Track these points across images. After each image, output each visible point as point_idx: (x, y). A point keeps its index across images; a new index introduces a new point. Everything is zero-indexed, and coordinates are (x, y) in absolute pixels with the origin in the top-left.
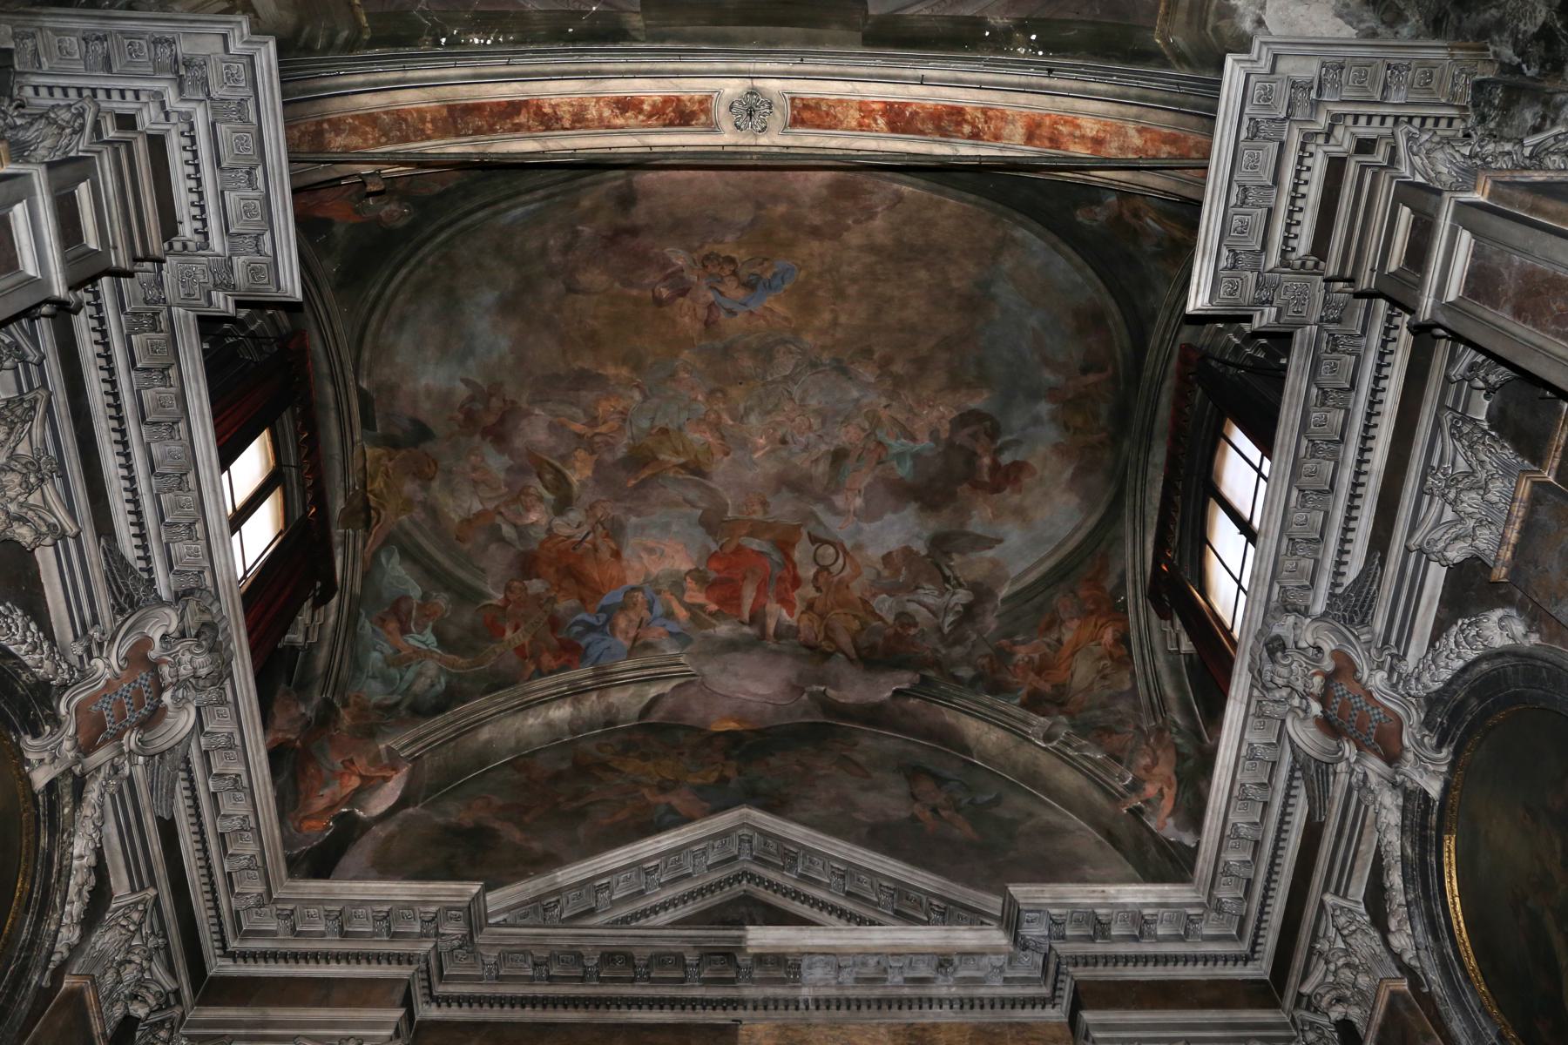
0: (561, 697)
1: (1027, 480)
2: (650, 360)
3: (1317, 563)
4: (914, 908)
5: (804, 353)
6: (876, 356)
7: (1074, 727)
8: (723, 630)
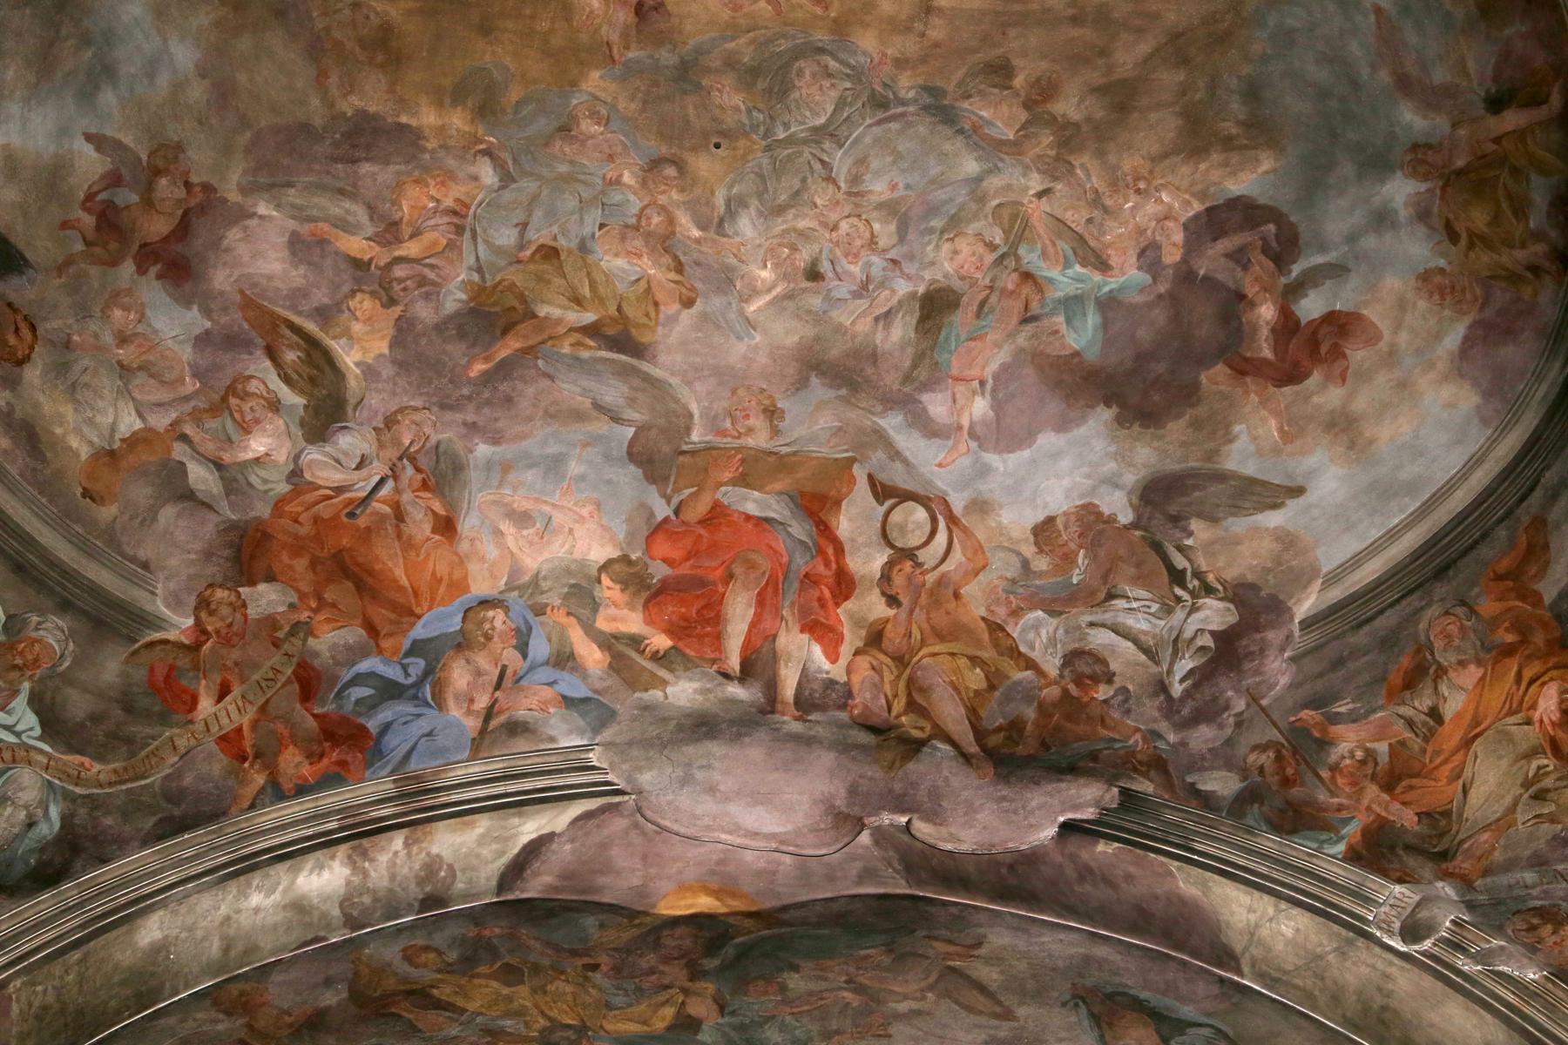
0: (327, 843)
1: (1357, 355)
2: (514, 94)
5: (857, 75)
6: (1019, 81)
7: (1470, 906)
8: (684, 692)
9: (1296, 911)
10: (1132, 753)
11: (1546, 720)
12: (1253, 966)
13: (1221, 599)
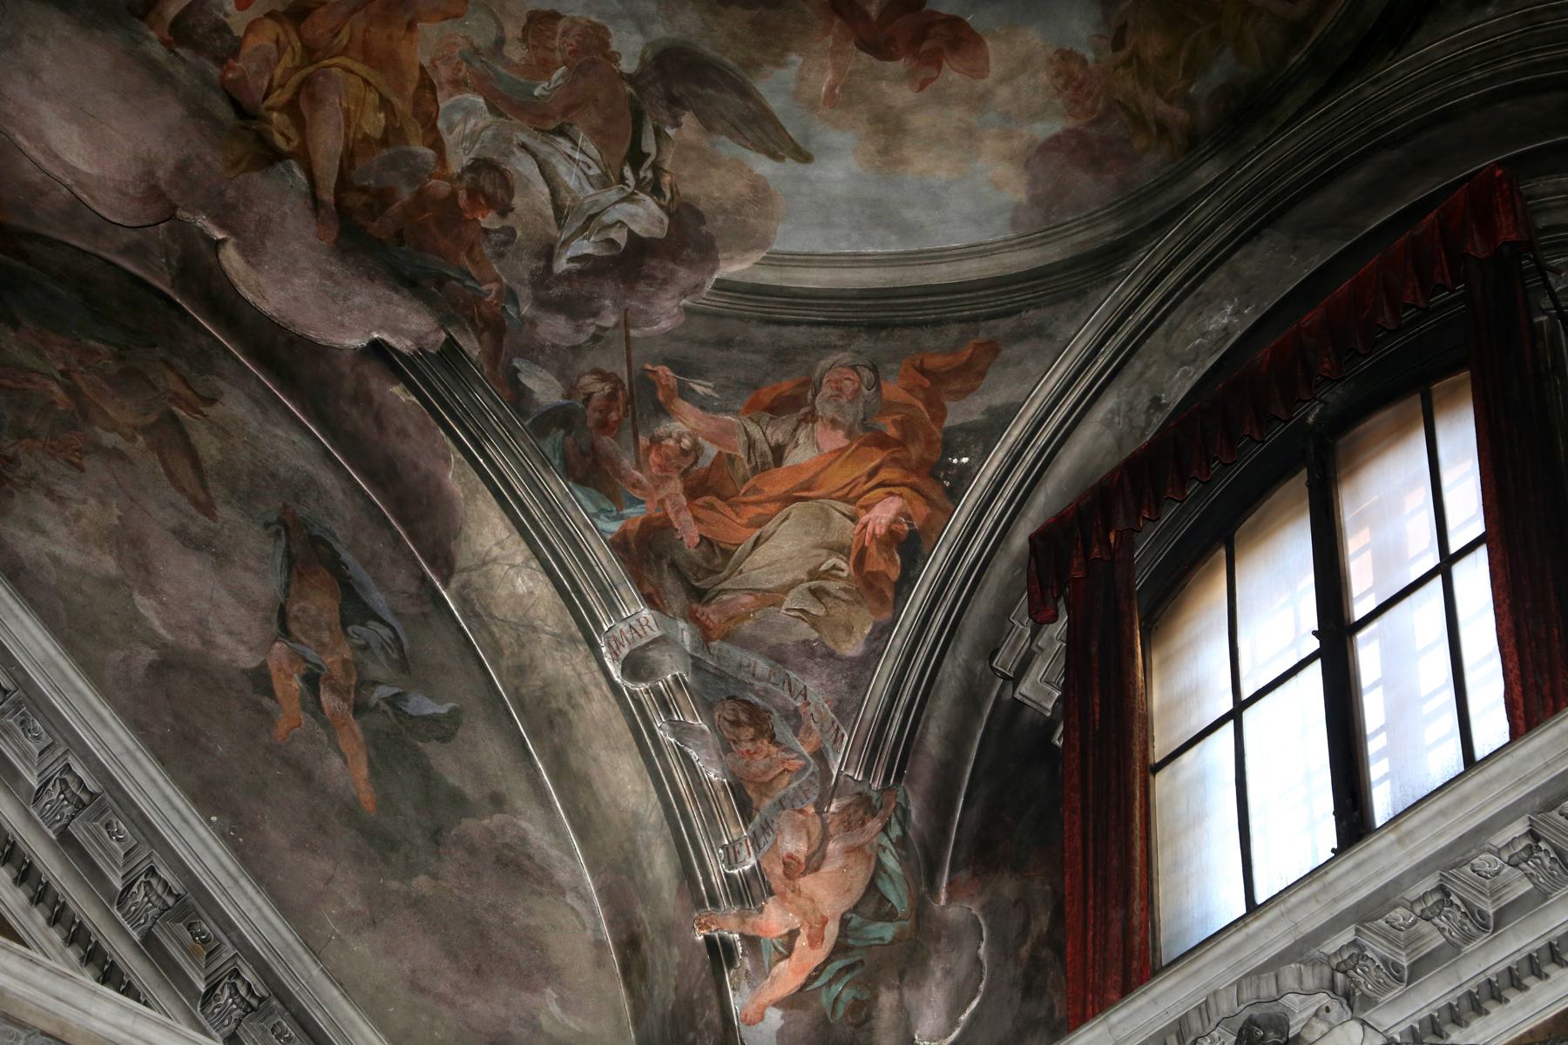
1: (952, 75)
3: (1451, 951)
4: (191, 953)
7: (697, 666)
9: (543, 577)
10: (479, 298)
11: (870, 528)
12: (463, 587)
13: (661, 207)
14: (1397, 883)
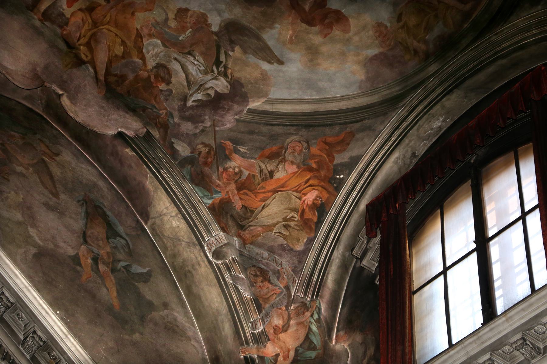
1: (337, 32)
7: (241, 254)
9: (183, 220)
10: (158, 116)
11: (306, 202)
12: (153, 224)
13: (227, 81)
14: (506, 336)
